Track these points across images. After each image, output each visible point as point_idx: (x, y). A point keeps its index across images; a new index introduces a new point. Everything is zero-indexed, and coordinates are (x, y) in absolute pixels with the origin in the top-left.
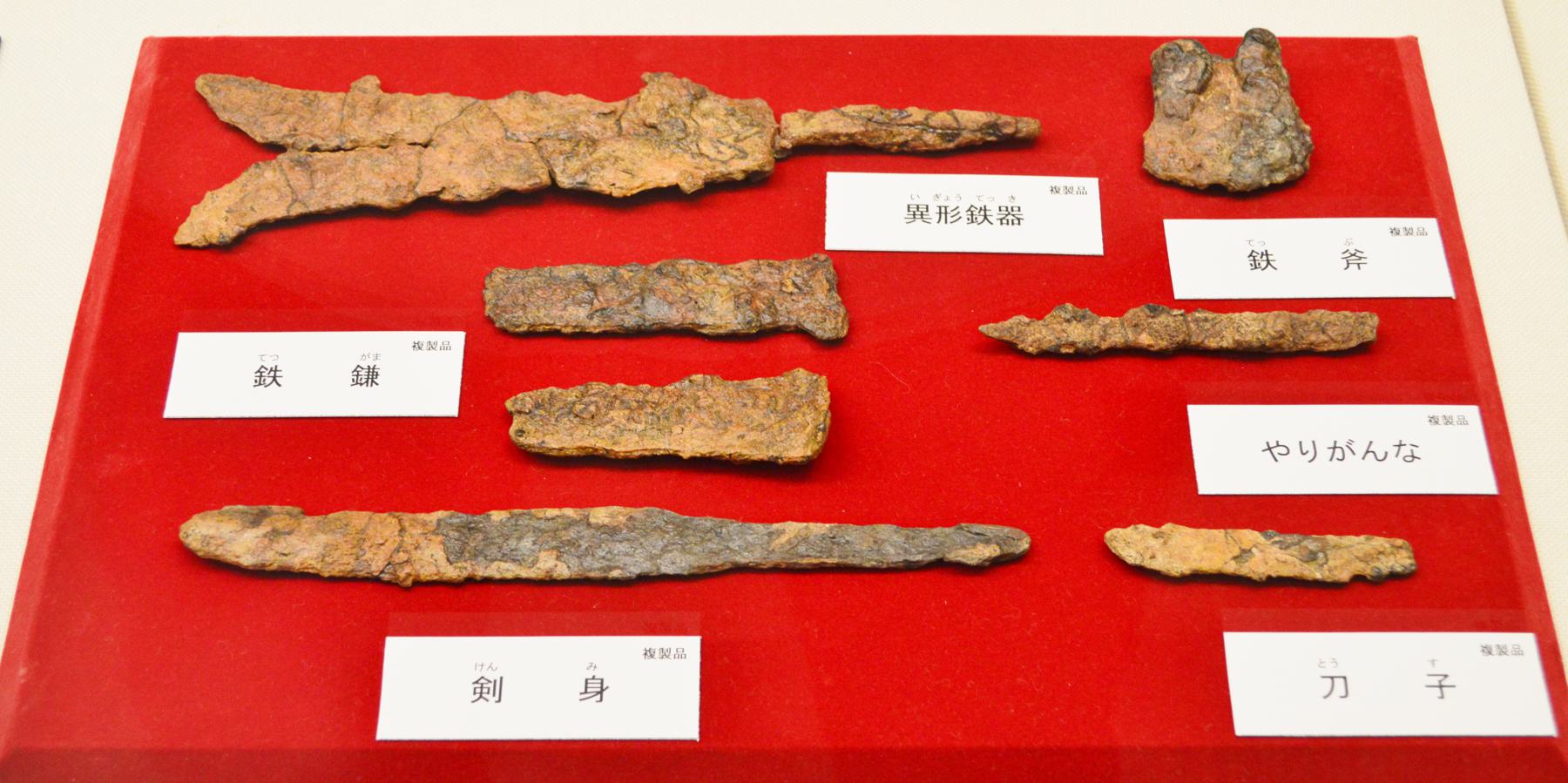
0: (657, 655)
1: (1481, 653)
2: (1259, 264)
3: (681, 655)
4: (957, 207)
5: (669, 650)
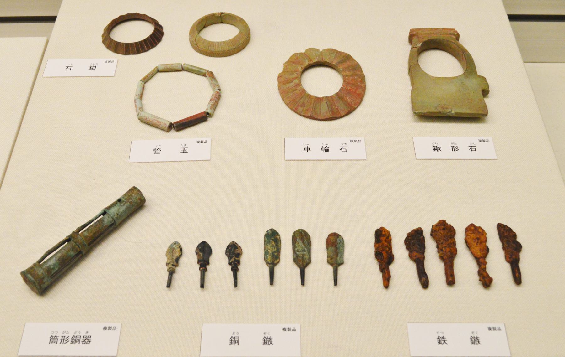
2: (441, 342)
4: (68, 337)
5: (111, 327)
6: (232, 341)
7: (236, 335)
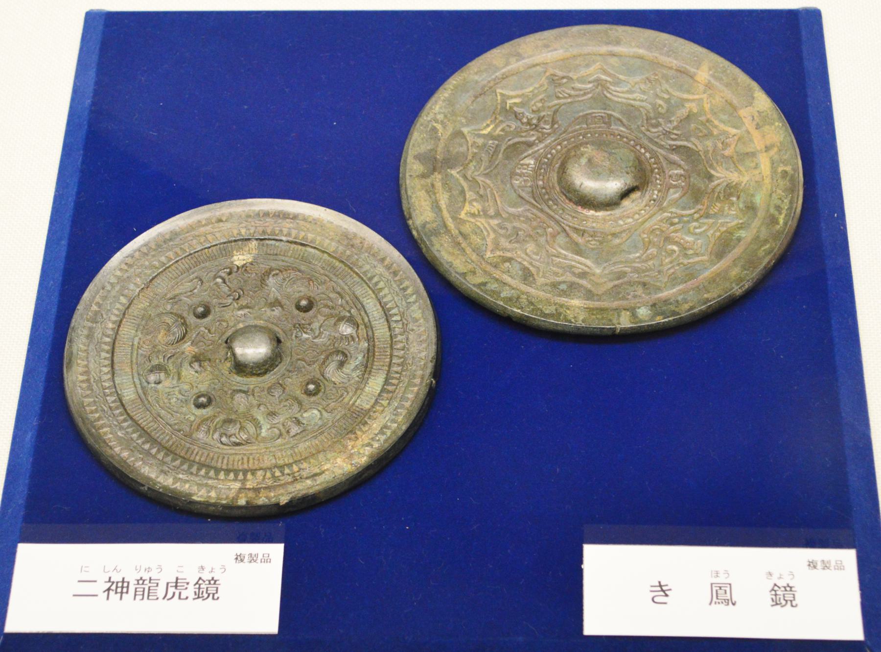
0: (246, 560)
1: (808, 567)
3: (267, 560)
5: (257, 555)
6: (199, 588)
7: (722, 579)
